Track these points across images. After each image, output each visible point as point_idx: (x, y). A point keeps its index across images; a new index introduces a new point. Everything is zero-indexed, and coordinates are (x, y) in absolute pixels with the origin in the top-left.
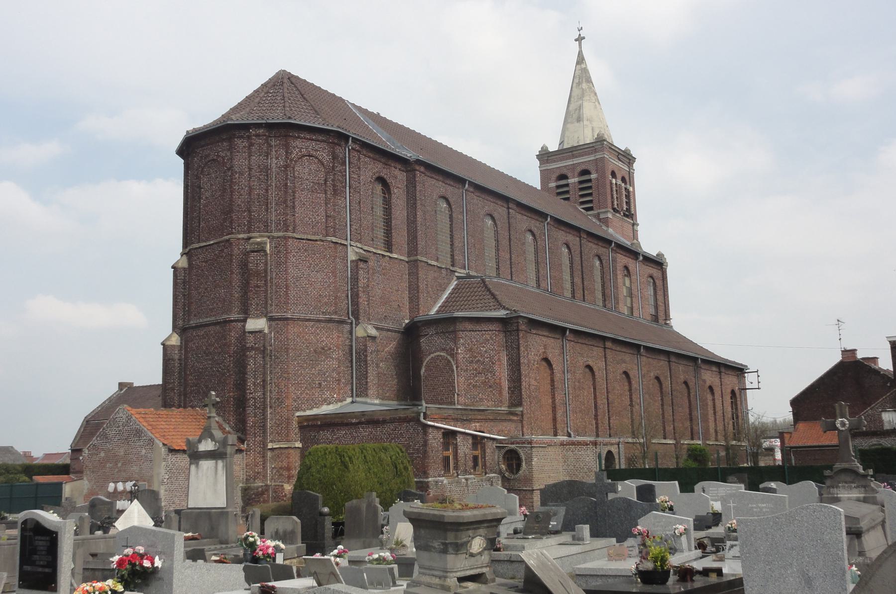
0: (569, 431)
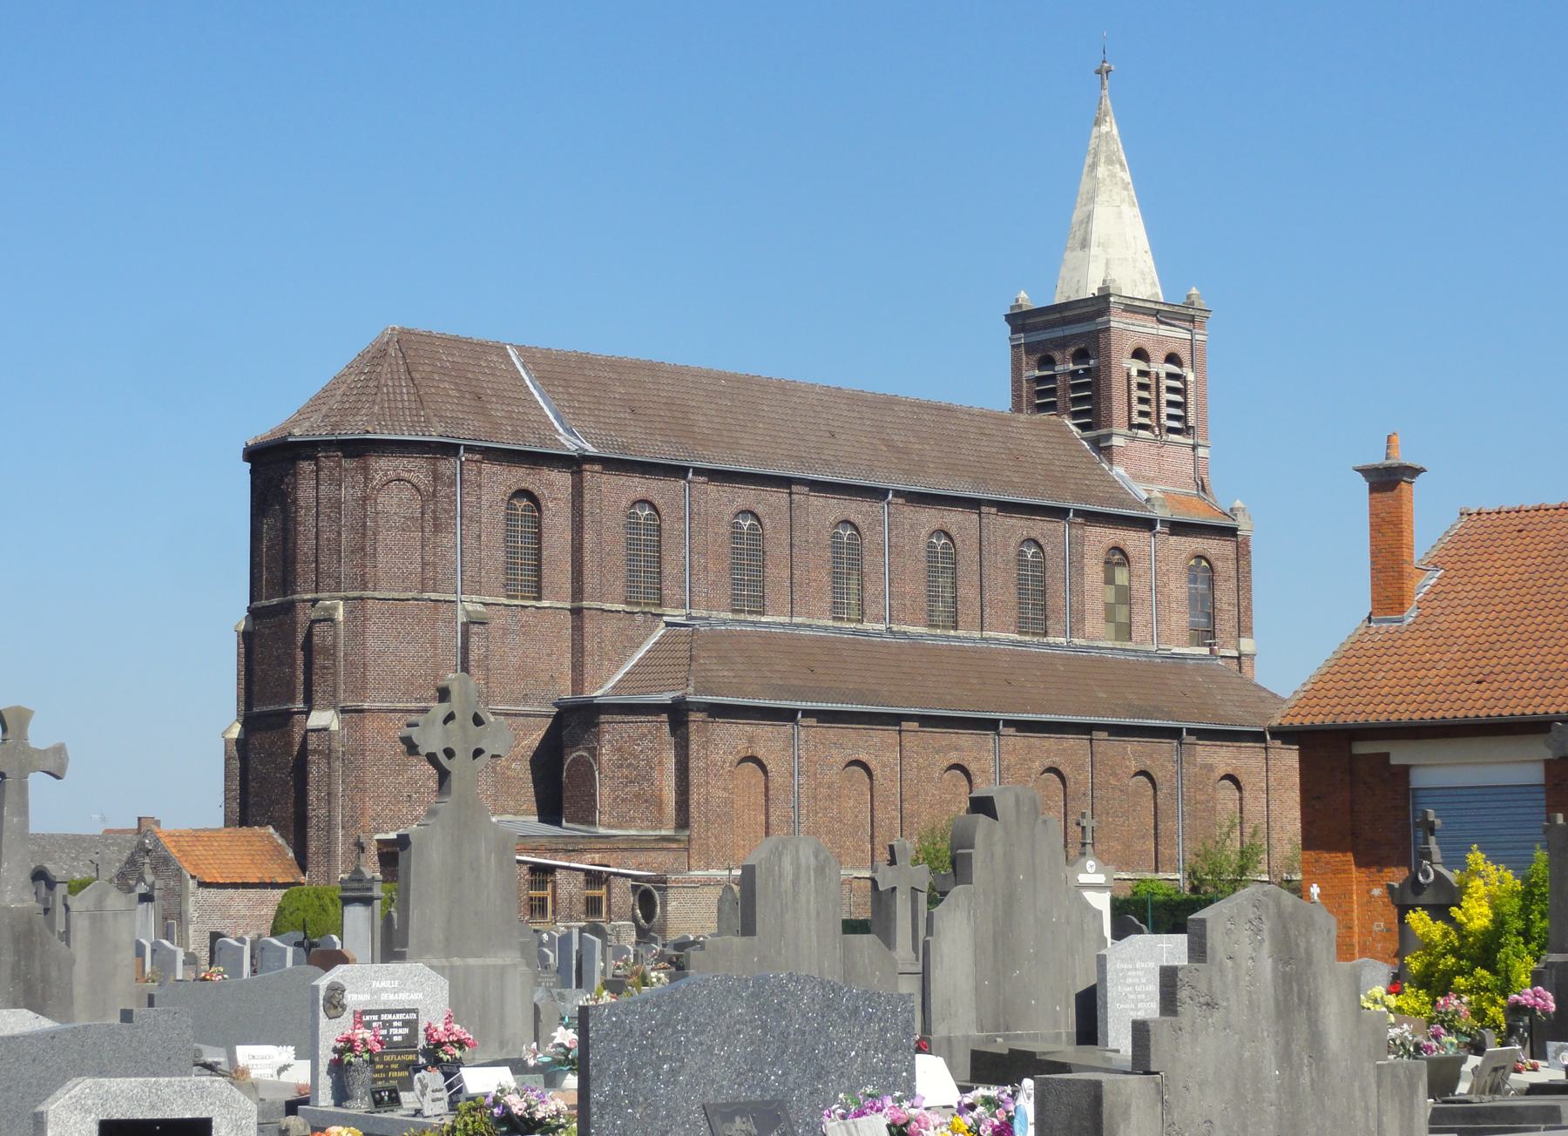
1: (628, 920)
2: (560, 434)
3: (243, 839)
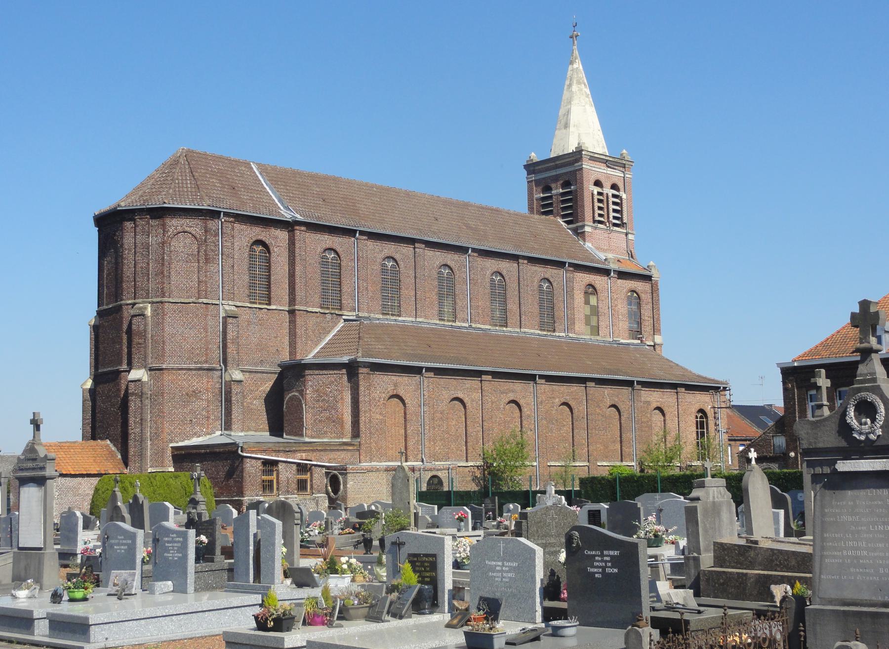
0: (423, 457)
2: (281, 210)
3: (90, 447)
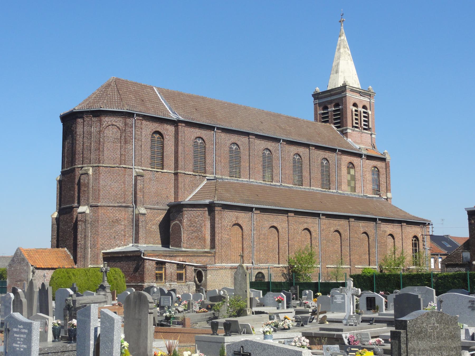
0: (253, 261)
1: (193, 282)
